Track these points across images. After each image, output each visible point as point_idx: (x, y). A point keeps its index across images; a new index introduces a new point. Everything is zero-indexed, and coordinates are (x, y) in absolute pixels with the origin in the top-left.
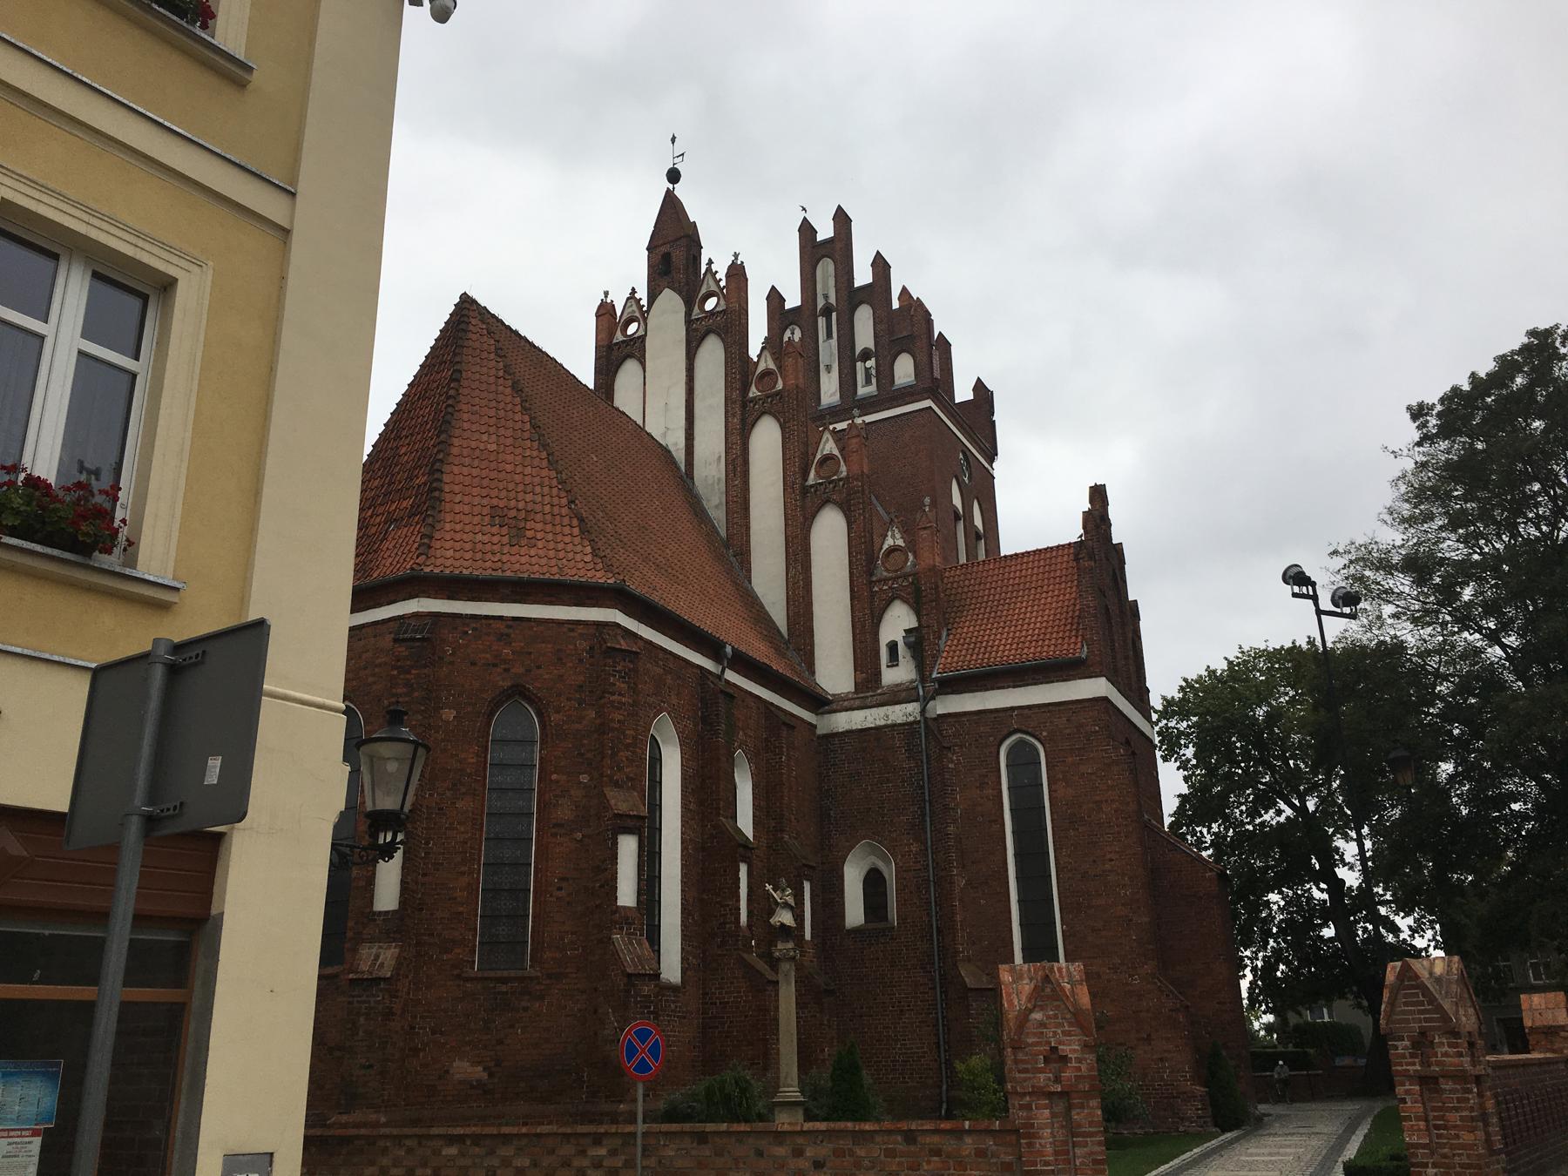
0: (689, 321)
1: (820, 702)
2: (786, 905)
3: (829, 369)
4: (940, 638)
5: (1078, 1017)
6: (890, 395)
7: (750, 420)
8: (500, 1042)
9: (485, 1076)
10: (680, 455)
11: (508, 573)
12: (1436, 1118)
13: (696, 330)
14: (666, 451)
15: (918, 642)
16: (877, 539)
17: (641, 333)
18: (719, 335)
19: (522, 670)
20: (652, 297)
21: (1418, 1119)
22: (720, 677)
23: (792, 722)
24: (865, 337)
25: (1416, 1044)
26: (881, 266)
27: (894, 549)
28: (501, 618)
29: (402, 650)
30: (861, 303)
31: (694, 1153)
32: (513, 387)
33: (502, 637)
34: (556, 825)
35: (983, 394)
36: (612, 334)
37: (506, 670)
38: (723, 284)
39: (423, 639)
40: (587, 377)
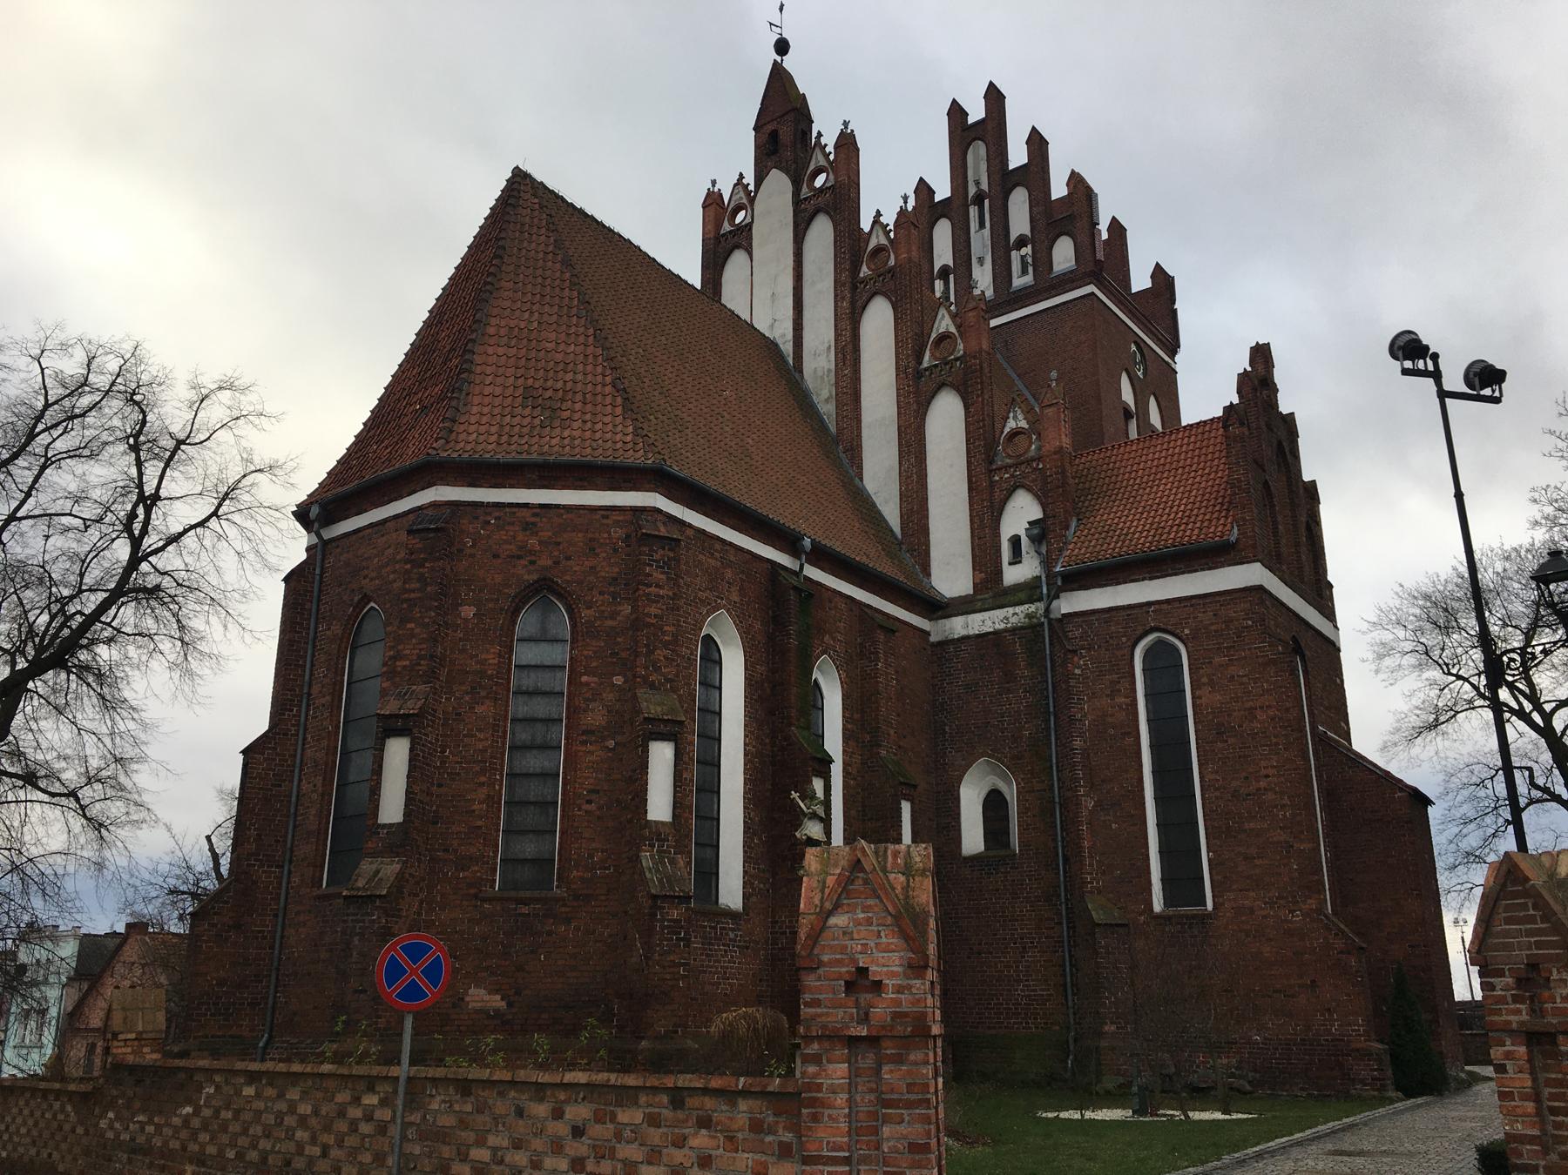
0: (797, 202)
1: (937, 608)
2: (814, 816)
3: (981, 261)
4: (1067, 528)
5: (906, 922)
7: (859, 304)
10: (787, 348)
11: (534, 456)
12: (1553, 1097)
14: (771, 346)
15: (1040, 532)
16: (998, 426)
17: (748, 220)
18: (827, 213)
19: (550, 562)
20: (759, 180)
21: (1524, 1097)
22: (797, 574)
23: (891, 626)
24: (1020, 221)
25: (1521, 982)
26: (1037, 142)
27: (1016, 433)
28: (526, 505)
30: (1014, 187)
31: (457, 1107)
32: (563, 262)
33: (527, 526)
34: (584, 733)
35: (1163, 282)
36: (719, 225)
37: (533, 563)
38: (832, 157)
39: (437, 530)
40: (694, 276)
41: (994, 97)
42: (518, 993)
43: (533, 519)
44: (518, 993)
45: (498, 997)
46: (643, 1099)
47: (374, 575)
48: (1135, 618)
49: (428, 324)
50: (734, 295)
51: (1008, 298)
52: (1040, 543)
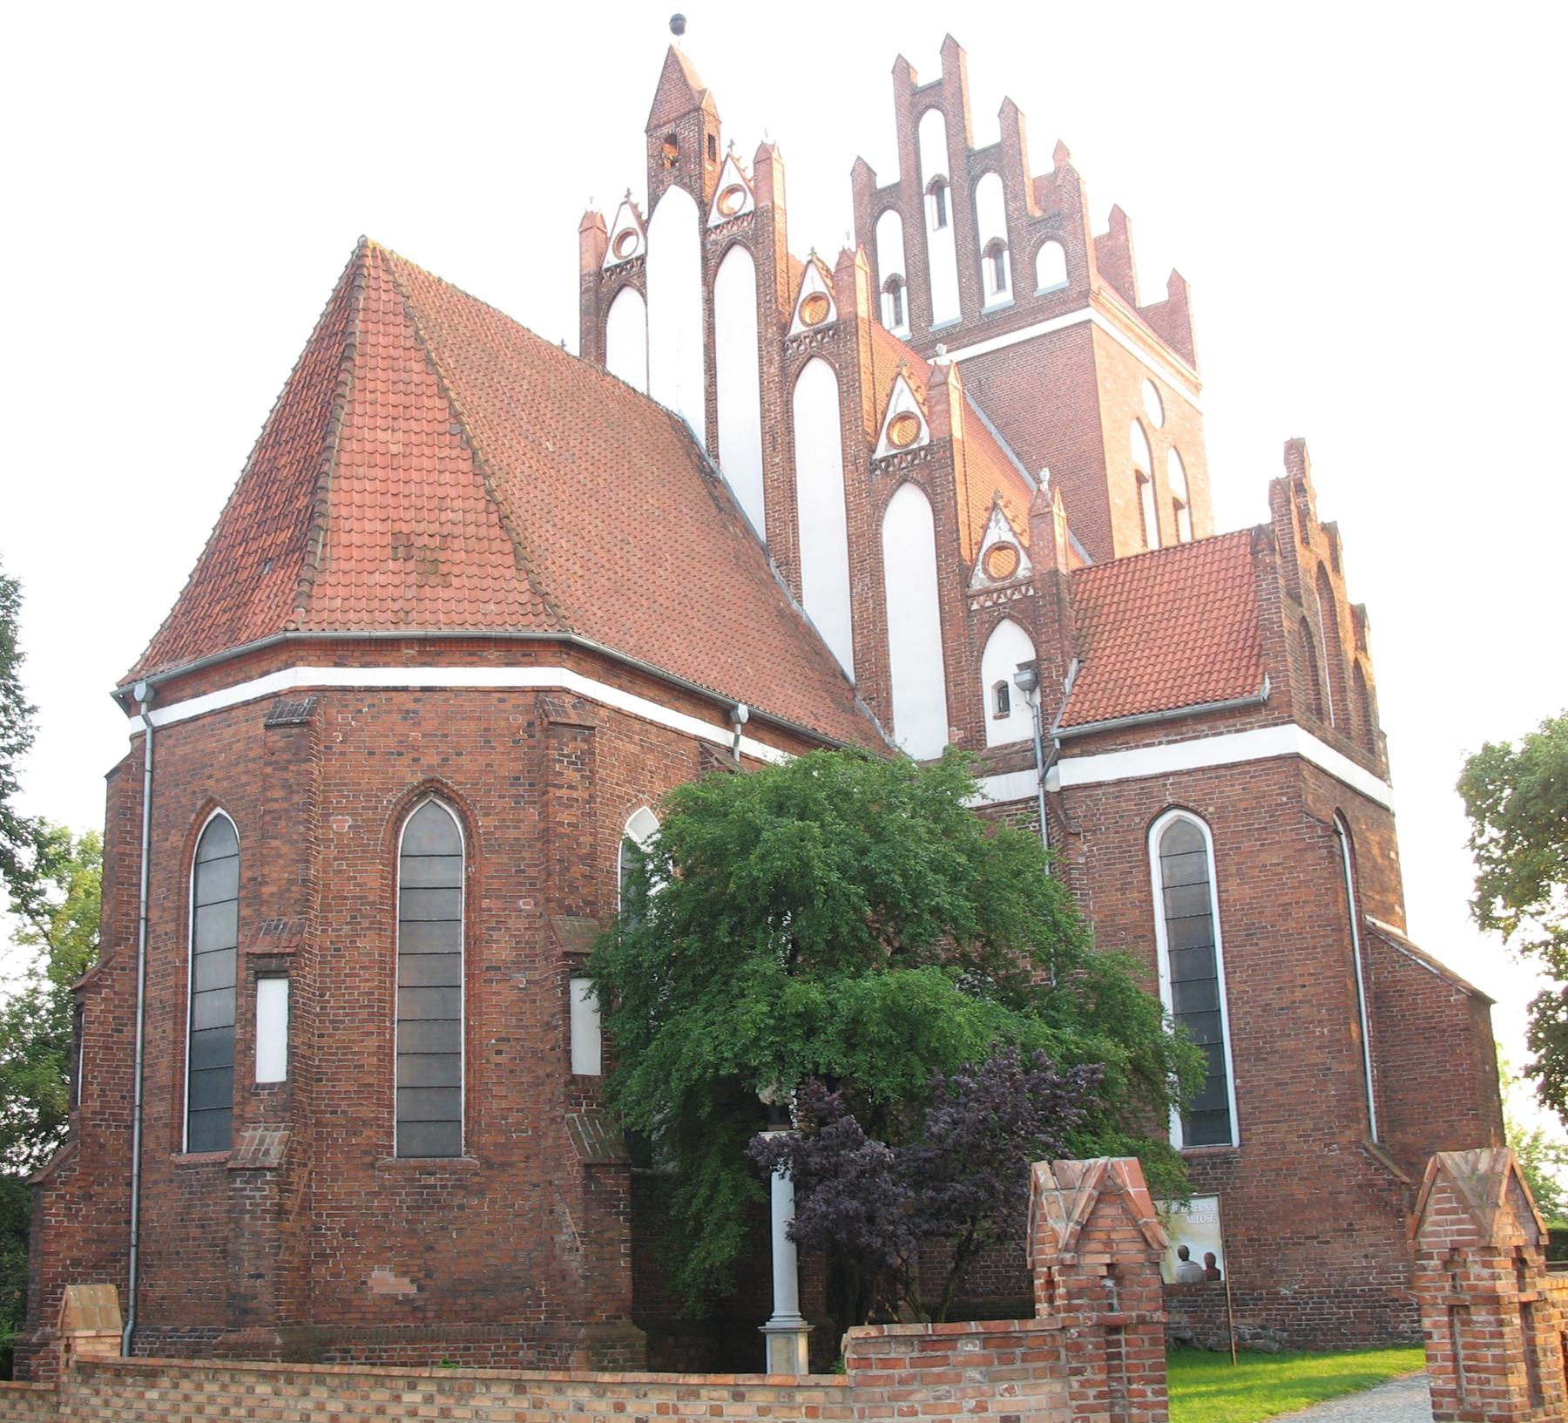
4: (1065, 675)
6: (1029, 307)
7: (793, 369)
8: (430, 1248)
9: (412, 1290)
12: (1467, 1358)
13: (715, 243)
14: (679, 426)
15: (1038, 675)
17: (640, 251)
18: (747, 248)
19: (436, 760)
20: (654, 201)
22: (731, 751)
24: (992, 223)
25: (1447, 1264)
26: (1010, 114)
29: (276, 738)
39: (302, 724)
41: (951, 49)
42: (428, 1276)
43: (412, 706)
44: (428, 1276)
45: (407, 1280)
46: (704, 1392)
47: (219, 774)
48: (1148, 795)
49: (262, 446)
50: (623, 361)
51: (977, 324)
52: (1032, 691)
